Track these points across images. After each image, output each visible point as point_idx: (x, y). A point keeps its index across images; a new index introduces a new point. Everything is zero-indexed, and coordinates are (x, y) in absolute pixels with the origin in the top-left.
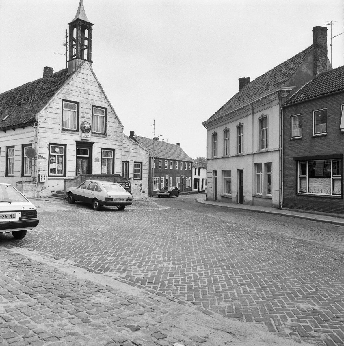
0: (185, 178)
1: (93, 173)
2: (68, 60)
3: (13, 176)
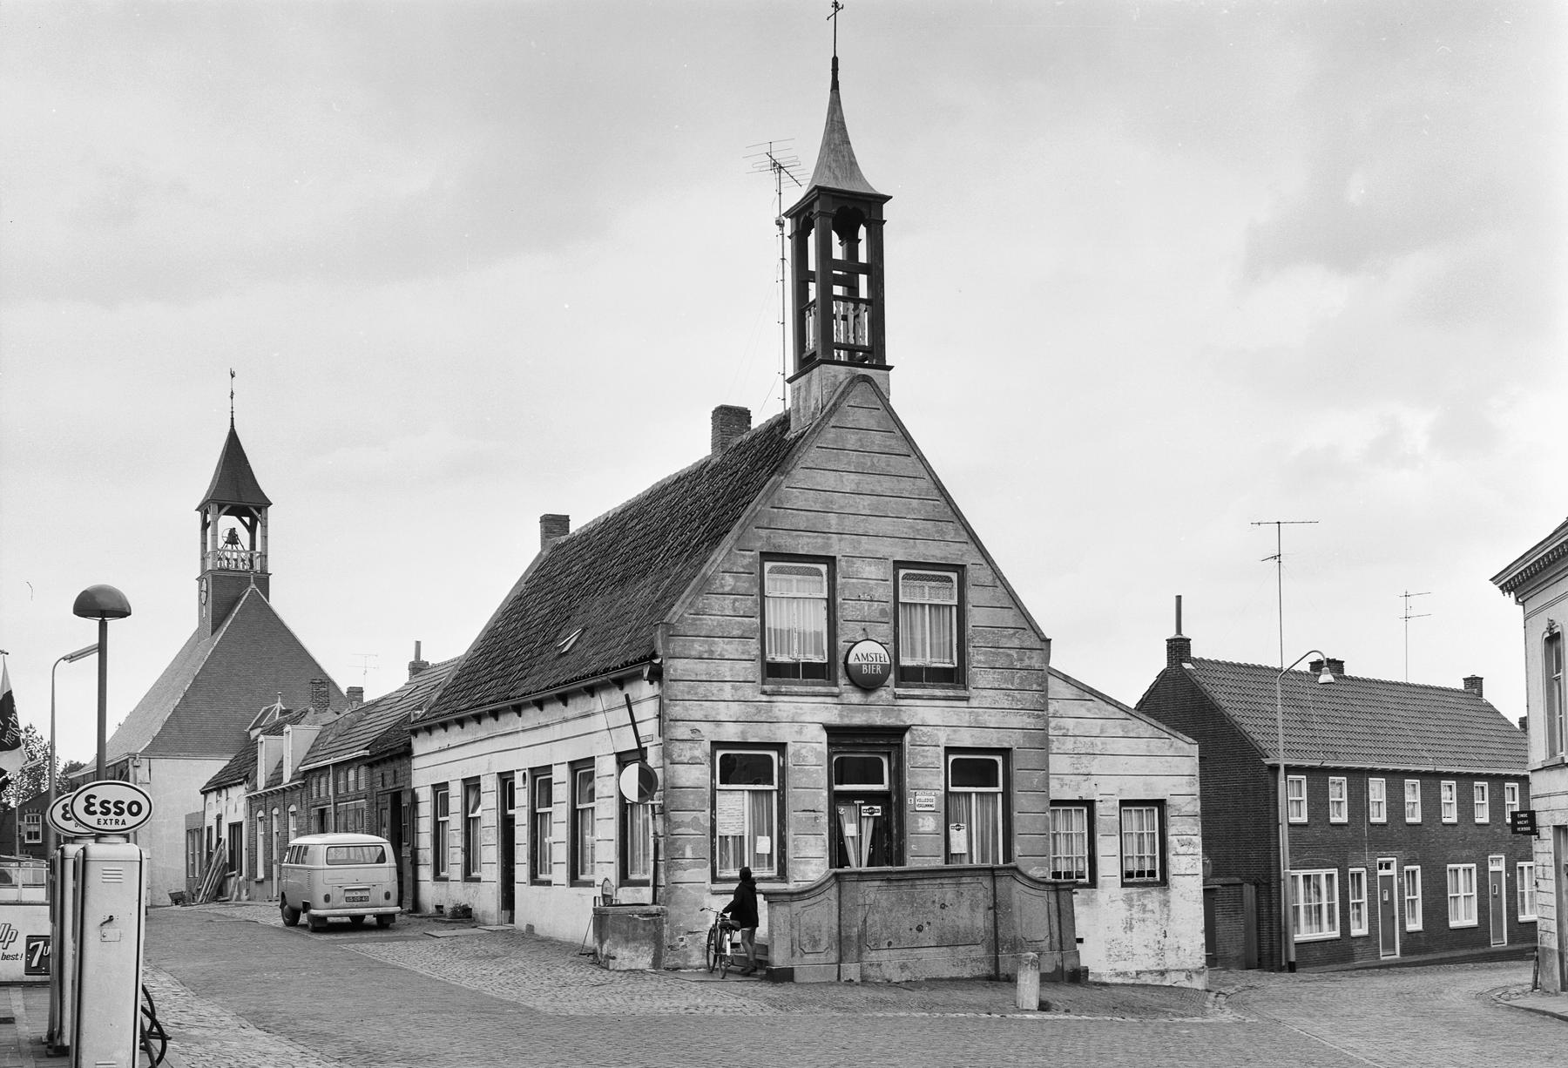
0: (1511, 868)
1: (912, 863)
2: (790, 373)
3: (549, 883)
